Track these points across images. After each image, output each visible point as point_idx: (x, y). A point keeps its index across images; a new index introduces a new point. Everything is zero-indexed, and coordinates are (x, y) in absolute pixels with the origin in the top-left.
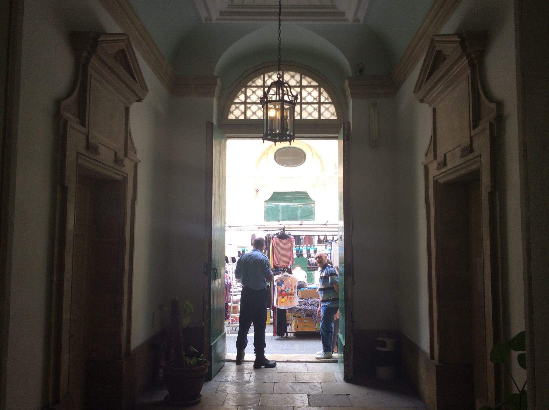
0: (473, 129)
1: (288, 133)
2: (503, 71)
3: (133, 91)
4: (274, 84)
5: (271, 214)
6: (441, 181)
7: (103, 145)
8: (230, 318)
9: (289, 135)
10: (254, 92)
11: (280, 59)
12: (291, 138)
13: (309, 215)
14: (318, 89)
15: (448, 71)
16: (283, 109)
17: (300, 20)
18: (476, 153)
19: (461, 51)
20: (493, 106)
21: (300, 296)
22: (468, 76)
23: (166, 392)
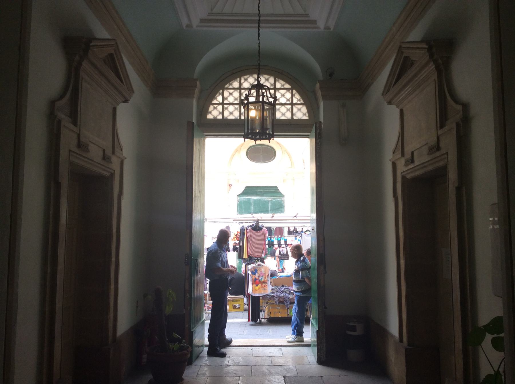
0: (440, 129)
2: (473, 74)
3: (121, 93)
4: (253, 87)
5: (243, 208)
6: (409, 176)
8: (207, 306)
9: (269, 134)
10: (231, 94)
11: (259, 64)
12: (270, 137)
13: (279, 208)
14: (291, 91)
15: (416, 75)
16: (263, 110)
17: (270, 27)
18: (443, 151)
19: (428, 57)
20: (459, 107)
21: (273, 284)
22: (435, 80)
23: (150, 377)
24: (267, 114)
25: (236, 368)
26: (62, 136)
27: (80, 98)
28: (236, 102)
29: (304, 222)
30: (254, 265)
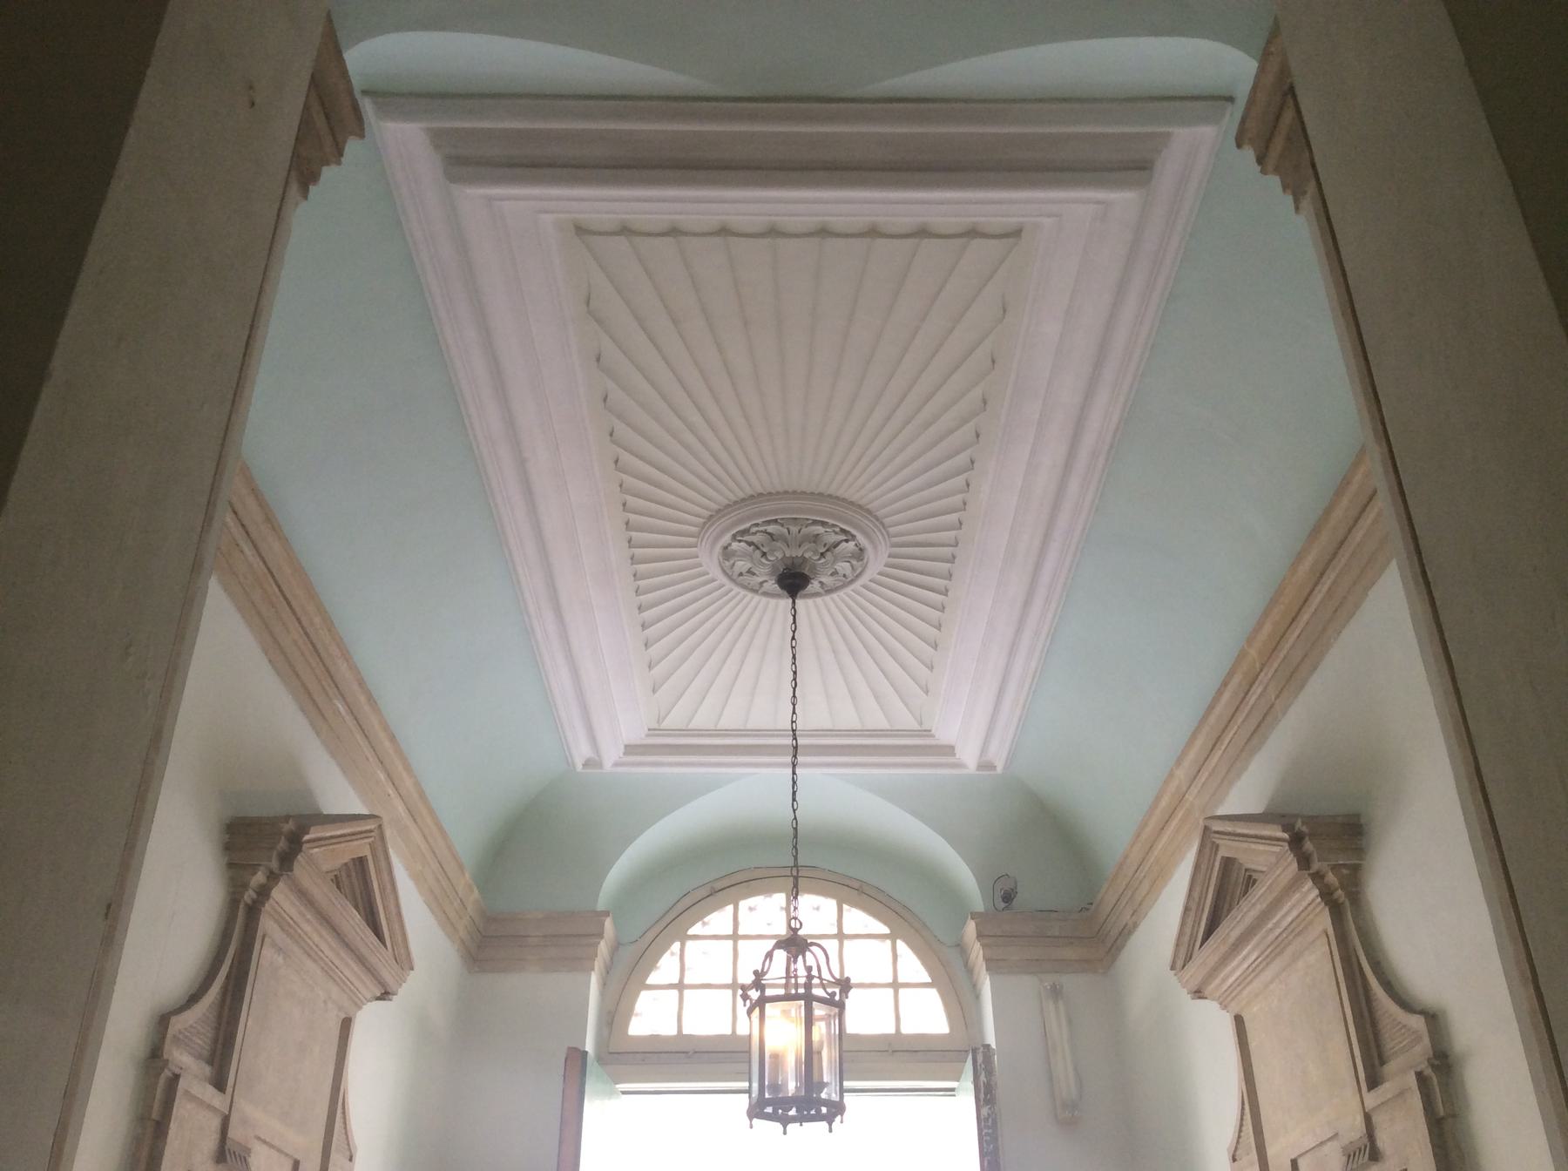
1: (823, 1095)
2: (1437, 912)
7: (265, 1142)
19: (1295, 865)
26: (173, 1126)
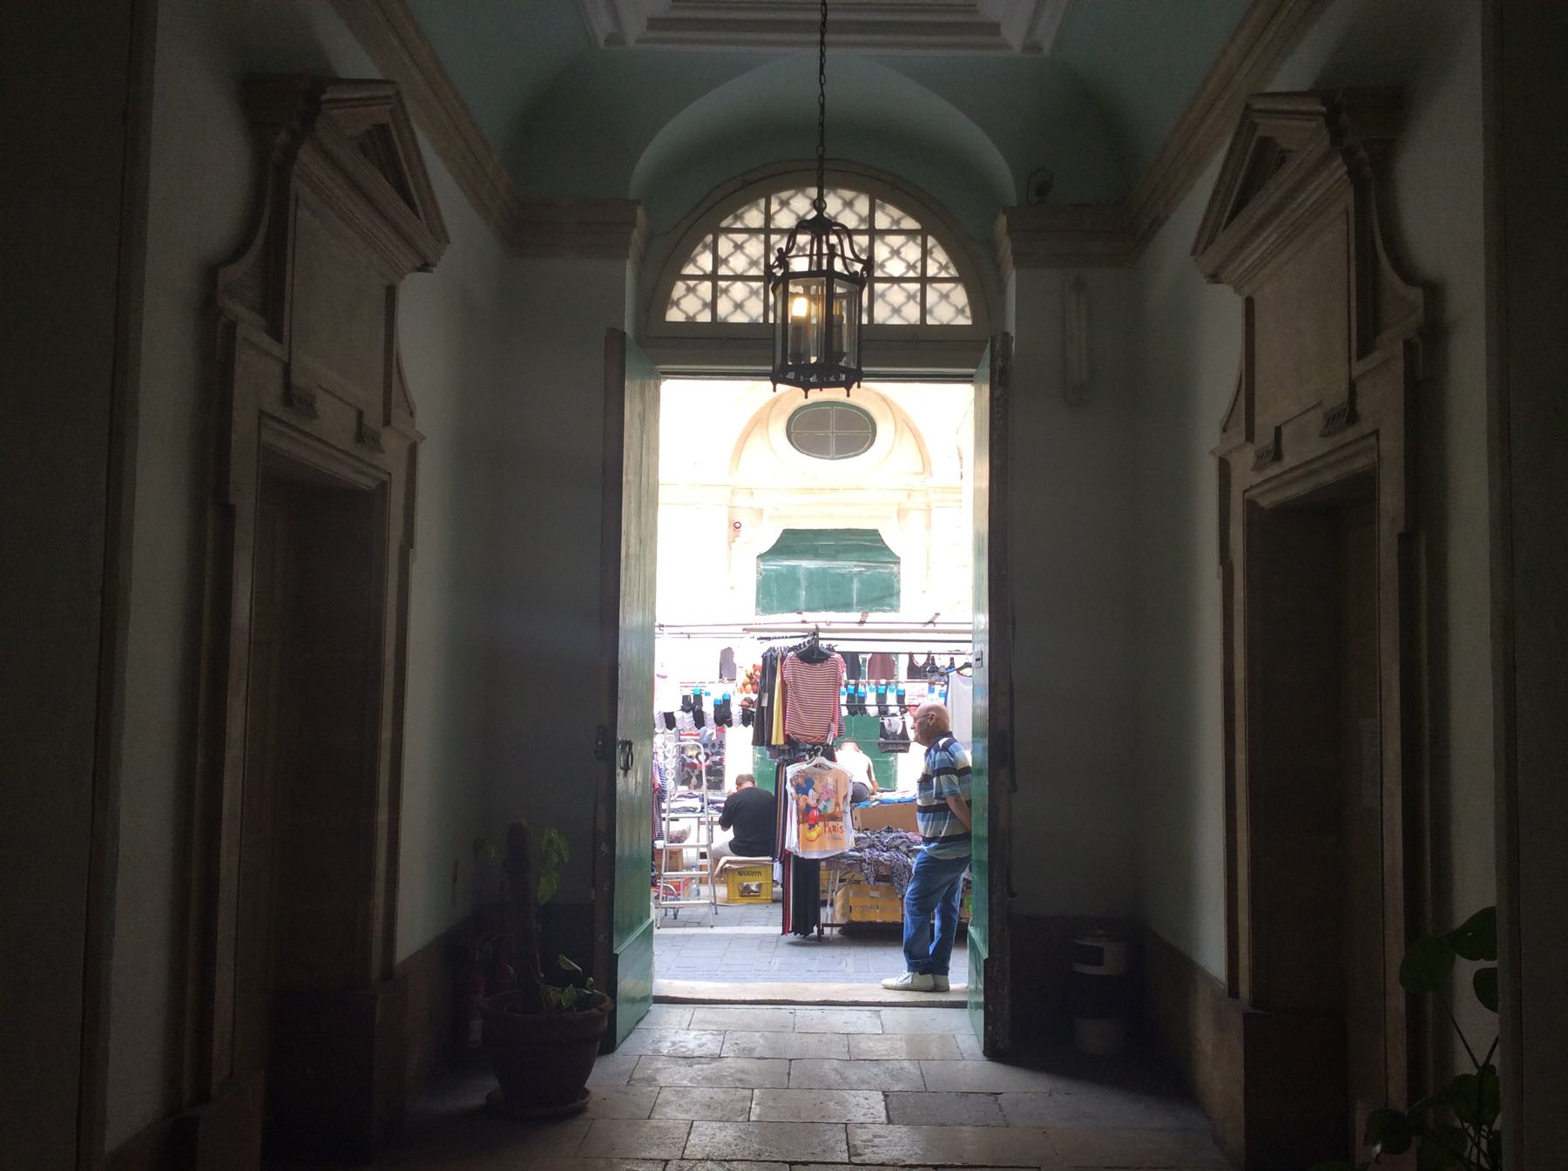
1: (842, 364)
4: (802, 225)
5: (774, 593)
6: (1266, 502)
7: (327, 391)
8: (661, 883)
9: (846, 370)
10: (738, 247)
12: (852, 378)
13: (883, 598)
14: (919, 240)
16: (830, 298)
17: (855, 44)
18: (1365, 427)
20: (1415, 295)
21: (858, 823)
22: (1347, 210)
24: (841, 309)
25: (742, 1063)
27: (289, 259)
28: (754, 272)
29: (952, 635)
30: (803, 766)
